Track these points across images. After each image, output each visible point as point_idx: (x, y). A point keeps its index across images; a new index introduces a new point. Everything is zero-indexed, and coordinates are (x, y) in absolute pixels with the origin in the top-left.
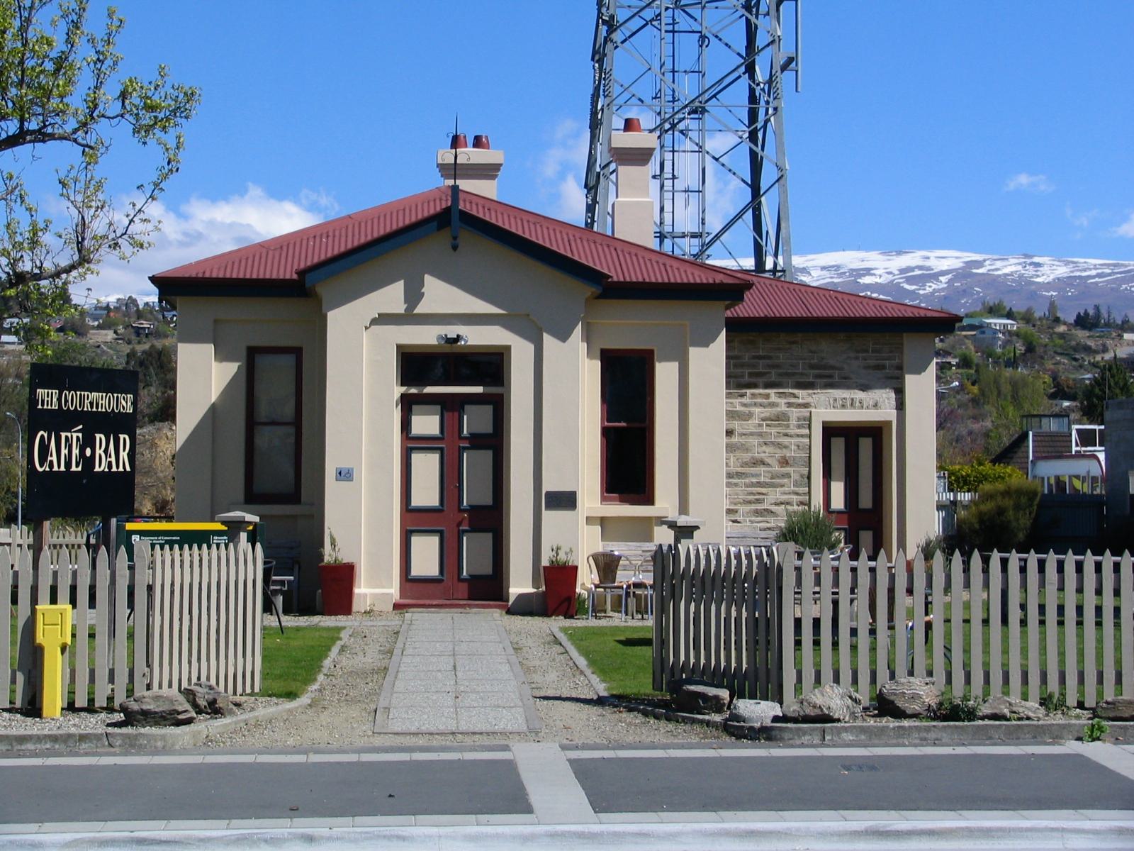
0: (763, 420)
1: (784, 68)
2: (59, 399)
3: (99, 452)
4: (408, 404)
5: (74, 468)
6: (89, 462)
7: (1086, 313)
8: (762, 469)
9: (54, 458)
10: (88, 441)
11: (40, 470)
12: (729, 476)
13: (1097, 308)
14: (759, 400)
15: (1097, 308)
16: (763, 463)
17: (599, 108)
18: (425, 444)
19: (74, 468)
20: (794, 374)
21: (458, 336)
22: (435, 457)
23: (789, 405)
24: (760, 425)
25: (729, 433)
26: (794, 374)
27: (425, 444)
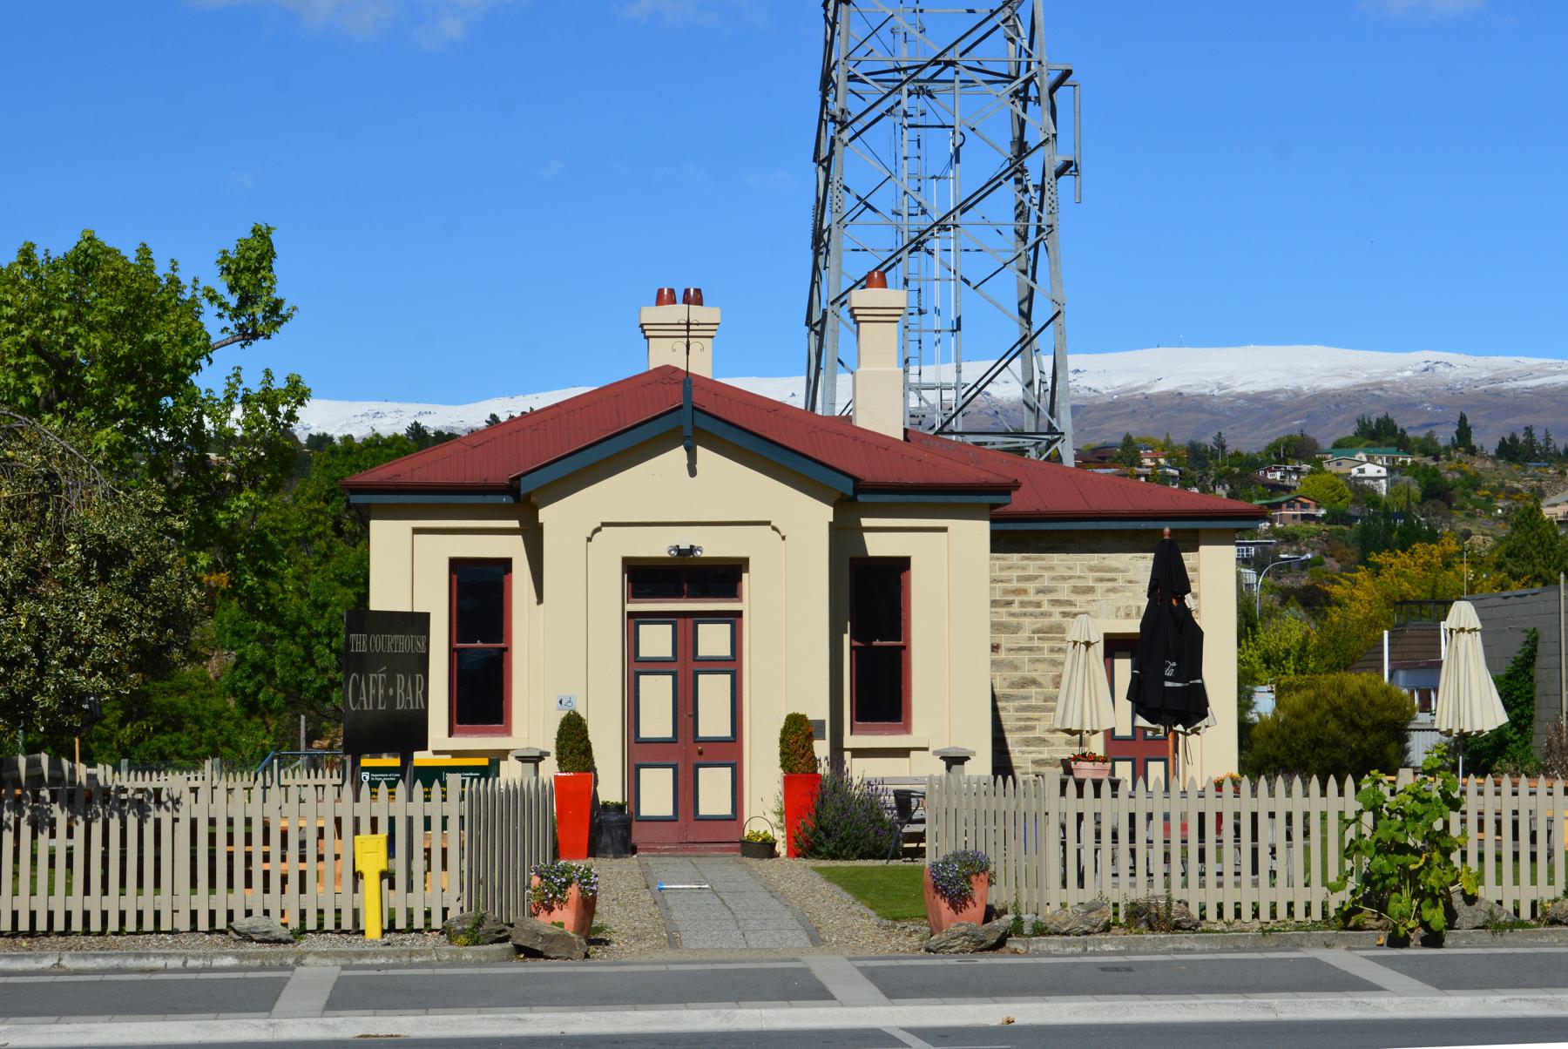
0: (1034, 632)
1: (1059, 173)
2: (368, 643)
3: (399, 691)
4: (634, 621)
5: (380, 708)
6: (391, 700)
7: (1514, 439)
8: (1033, 690)
9: (364, 698)
10: (390, 682)
11: (354, 709)
12: (994, 603)
13: (1529, 431)
14: (1030, 609)
15: (1529, 431)
16: (1034, 682)
17: (825, 227)
18: (656, 666)
19: (380, 708)
20: (1070, 578)
21: (692, 547)
22: (667, 680)
23: (1065, 614)
24: (1031, 639)
25: (995, 648)
26: (1070, 578)
27: (656, 666)
